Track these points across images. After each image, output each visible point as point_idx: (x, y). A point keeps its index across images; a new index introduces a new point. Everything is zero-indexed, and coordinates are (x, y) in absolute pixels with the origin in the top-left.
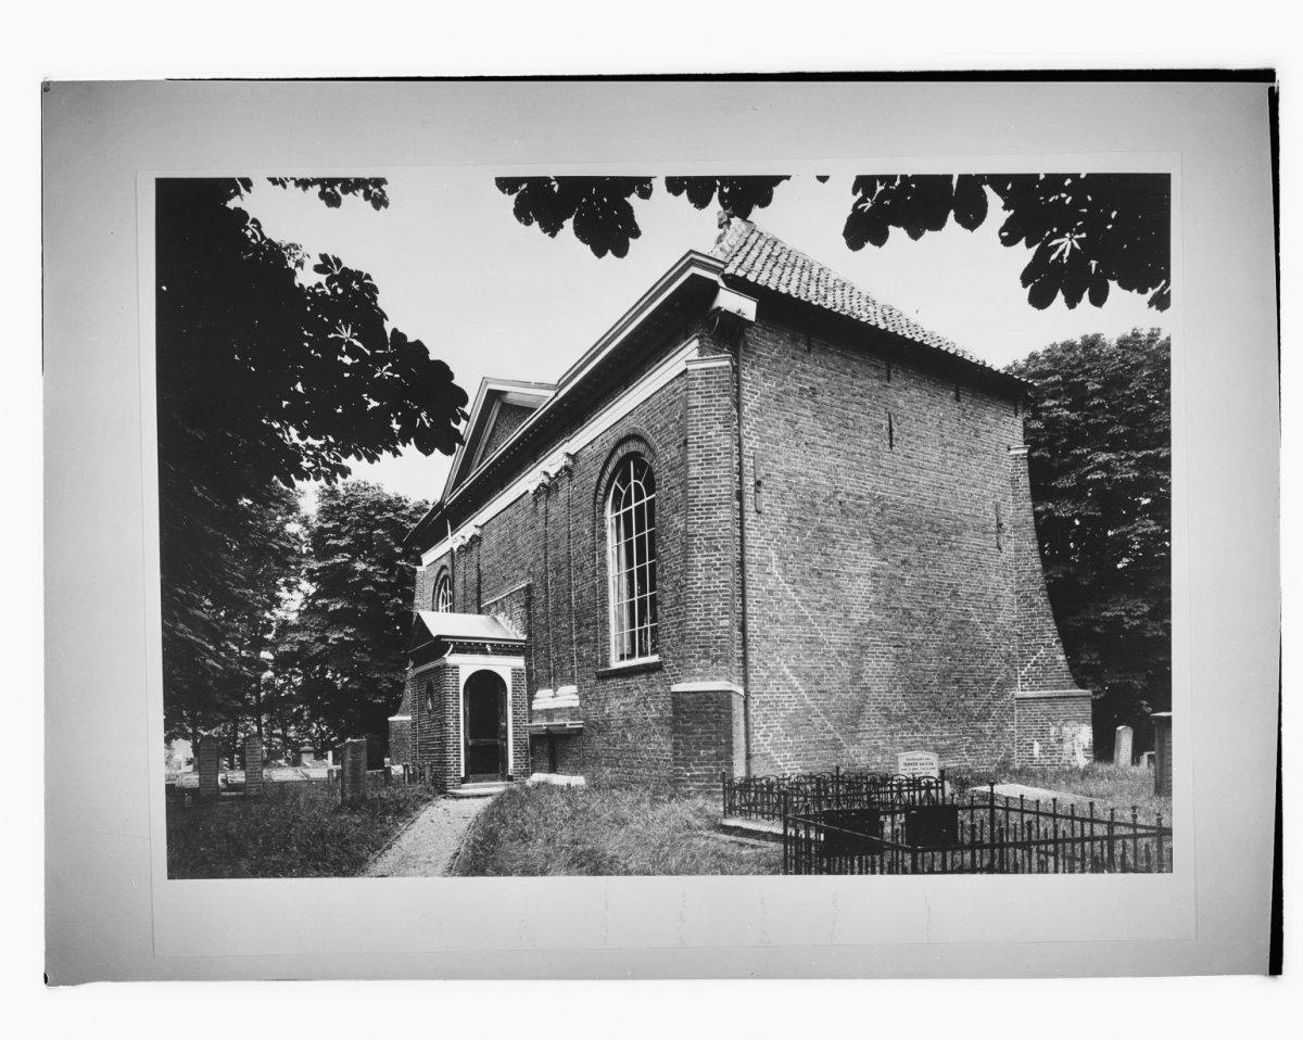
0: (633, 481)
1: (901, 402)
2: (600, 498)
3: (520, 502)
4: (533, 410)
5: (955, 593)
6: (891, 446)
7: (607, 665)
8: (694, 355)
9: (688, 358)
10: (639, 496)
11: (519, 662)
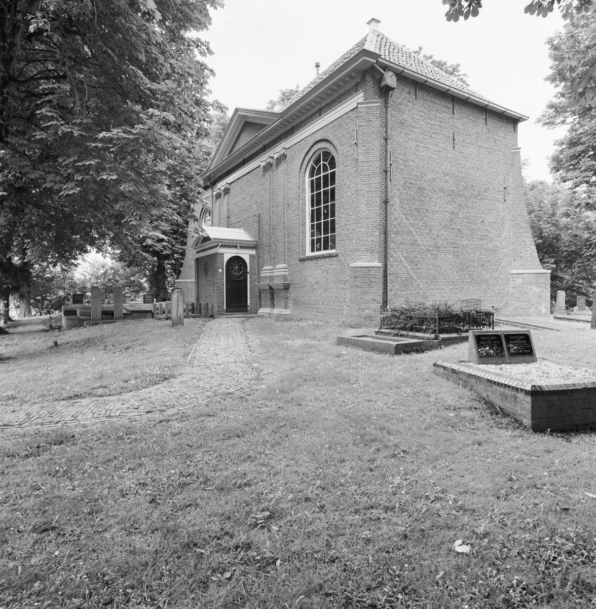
0: (322, 163)
1: (459, 125)
2: (303, 170)
3: (302, 142)
4: (263, 126)
5: (483, 222)
6: (454, 147)
7: (305, 255)
8: (361, 100)
9: (358, 101)
10: (325, 169)
11: (253, 252)
